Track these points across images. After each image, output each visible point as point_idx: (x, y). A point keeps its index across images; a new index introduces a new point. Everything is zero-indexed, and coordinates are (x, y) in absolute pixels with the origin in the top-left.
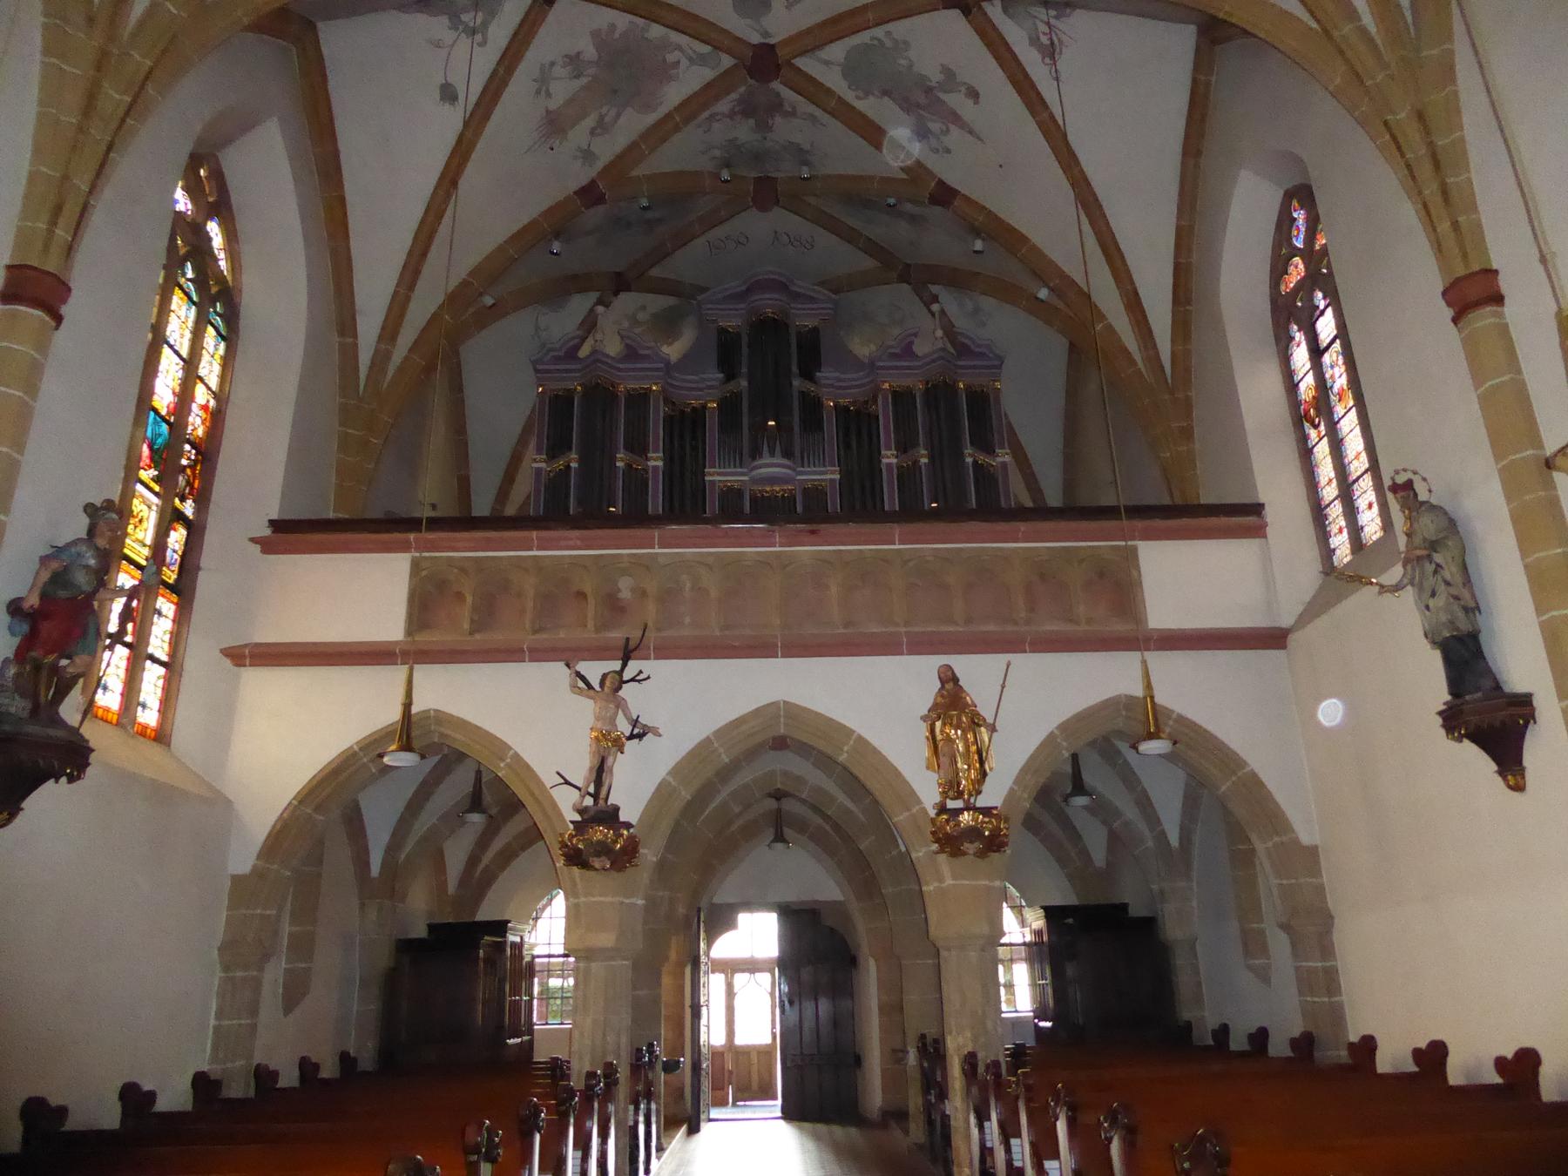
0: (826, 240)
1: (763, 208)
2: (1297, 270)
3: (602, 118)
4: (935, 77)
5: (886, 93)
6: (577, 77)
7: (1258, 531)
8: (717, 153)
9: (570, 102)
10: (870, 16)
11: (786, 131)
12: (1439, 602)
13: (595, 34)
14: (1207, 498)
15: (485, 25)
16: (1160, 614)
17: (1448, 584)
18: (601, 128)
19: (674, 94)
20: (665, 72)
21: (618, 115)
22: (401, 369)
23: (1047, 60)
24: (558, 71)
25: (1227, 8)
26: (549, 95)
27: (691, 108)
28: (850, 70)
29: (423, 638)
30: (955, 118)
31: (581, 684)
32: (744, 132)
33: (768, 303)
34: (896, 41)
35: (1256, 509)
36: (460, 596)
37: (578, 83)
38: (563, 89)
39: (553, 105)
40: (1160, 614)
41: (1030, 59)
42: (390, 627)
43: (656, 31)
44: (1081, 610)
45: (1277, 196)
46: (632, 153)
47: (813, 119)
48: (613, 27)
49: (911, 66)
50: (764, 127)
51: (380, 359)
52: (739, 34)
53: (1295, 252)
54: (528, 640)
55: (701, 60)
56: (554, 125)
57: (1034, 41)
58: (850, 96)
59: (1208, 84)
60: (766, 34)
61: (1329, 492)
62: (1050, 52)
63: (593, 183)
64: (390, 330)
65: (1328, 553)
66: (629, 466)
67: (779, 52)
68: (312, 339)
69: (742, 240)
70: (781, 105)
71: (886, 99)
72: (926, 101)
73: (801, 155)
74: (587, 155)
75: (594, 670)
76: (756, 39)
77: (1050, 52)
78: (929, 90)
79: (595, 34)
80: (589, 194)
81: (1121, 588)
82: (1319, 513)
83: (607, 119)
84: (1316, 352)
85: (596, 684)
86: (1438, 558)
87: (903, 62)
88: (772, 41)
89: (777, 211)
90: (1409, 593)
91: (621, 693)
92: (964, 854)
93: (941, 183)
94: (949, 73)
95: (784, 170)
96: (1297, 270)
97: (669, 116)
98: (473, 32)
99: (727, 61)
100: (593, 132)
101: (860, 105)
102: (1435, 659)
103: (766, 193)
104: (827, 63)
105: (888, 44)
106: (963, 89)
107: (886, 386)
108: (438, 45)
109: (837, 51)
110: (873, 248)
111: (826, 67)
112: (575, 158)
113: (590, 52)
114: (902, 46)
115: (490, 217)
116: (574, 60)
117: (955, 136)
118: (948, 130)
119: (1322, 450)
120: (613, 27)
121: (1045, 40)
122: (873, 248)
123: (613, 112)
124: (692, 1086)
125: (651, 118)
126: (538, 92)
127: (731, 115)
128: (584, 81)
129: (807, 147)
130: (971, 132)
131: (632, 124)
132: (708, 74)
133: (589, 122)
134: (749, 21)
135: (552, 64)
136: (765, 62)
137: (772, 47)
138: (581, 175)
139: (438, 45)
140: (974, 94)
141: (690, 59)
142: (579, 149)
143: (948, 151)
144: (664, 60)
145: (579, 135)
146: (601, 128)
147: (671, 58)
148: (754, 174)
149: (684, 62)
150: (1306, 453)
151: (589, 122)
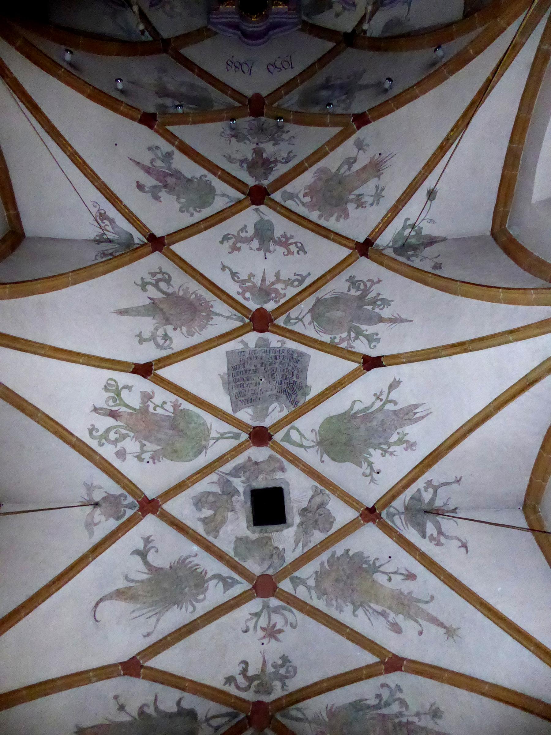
0: (216, 69)
1: (257, 96)
3: (349, 169)
4: (163, 194)
5: (190, 180)
6: (360, 195)
8: (285, 136)
9: (365, 182)
10: (202, 226)
11: (246, 150)
13: (347, 217)
15: (404, 228)
18: (350, 162)
19: (307, 178)
20: (311, 191)
21: (339, 169)
22: (516, 16)
23: (103, 212)
24: (370, 200)
25: (7, 290)
26: (377, 187)
28: (212, 191)
30: (148, 171)
32: (269, 149)
33: (254, 25)
34: (188, 211)
38: (368, 189)
41: (112, 212)
47: (230, 159)
48: (338, 220)
49: (178, 199)
50: (258, 152)
51: (525, 32)
52: (271, 211)
55: (292, 196)
56: (376, 167)
57: (112, 221)
58: (210, 176)
59: (7, 210)
60: (256, 210)
62: (103, 216)
63: (359, 128)
64: (514, 49)
67: (250, 202)
69: (271, 68)
70: (248, 168)
71: (189, 176)
72: (166, 181)
73: (236, 134)
74: (360, 146)
76: (262, 208)
79: (347, 217)
80: (362, 120)
83: (346, 167)
87: (183, 200)
88: (254, 207)
89: (249, 92)
92: (305, 195)
93: (151, 127)
94: (157, 198)
95: (245, 122)
97: (311, 166)
98: (413, 226)
100: (355, 160)
101: (204, 172)
103: (256, 106)
104: (224, 195)
105: (191, 209)
106: (147, 189)
109: (219, 204)
110: (189, 65)
111: (224, 195)
112: (368, 145)
113: (351, 207)
115: (424, 118)
116: (360, 204)
118: (151, 163)
120: (338, 220)
122: (189, 65)
123: (342, 171)
124: (233, 457)
125: (321, 164)
126: (383, 189)
127: (276, 162)
128: (357, 192)
129: (233, 140)
130: (138, 163)
131: (332, 162)
132: (288, 188)
133: (356, 167)
134: (266, 218)
135: (372, 205)
136: (258, 196)
137: (253, 203)
138: (366, 132)
140: (140, 187)
141: (297, 197)
142: (364, 150)
143: (150, 149)
144: (312, 198)
145: (363, 160)
146: (350, 162)
147: (308, 199)
148: (263, 119)
149: (301, 195)
151: (356, 167)
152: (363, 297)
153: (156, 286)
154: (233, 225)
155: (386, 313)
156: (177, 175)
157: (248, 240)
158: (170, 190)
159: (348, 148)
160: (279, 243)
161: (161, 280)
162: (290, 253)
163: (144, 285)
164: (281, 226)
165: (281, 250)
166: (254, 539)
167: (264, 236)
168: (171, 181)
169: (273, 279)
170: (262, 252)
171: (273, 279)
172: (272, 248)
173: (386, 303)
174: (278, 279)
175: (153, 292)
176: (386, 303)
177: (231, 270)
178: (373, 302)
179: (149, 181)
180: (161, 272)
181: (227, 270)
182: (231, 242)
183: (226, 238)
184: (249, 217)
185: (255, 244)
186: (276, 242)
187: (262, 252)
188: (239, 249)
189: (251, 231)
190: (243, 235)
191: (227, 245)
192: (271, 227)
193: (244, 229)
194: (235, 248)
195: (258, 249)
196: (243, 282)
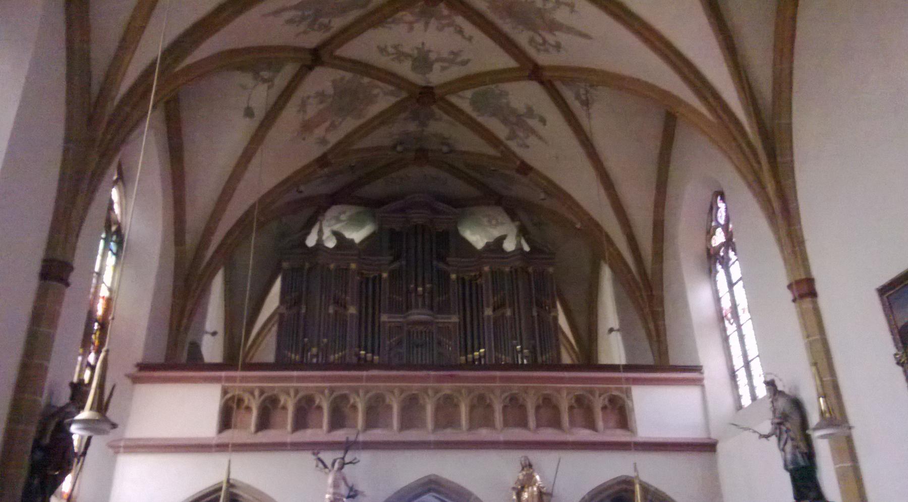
2: (719, 238)
6: (321, 102)
7: (698, 382)
12: (789, 447)
14: (672, 362)
16: (645, 431)
17: (792, 439)
27: (384, 118)
28: (473, 103)
29: (229, 436)
30: (533, 131)
31: (321, 465)
32: (412, 127)
35: (697, 369)
36: (248, 409)
37: (321, 107)
38: (312, 110)
39: (307, 117)
40: (647, 426)
41: (575, 106)
42: (206, 426)
43: (366, 80)
44: (600, 424)
45: (709, 194)
46: (349, 138)
48: (342, 79)
53: (718, 225)
54: (290, 438)
55: (392, 93)
56: (307, 127)
57: (578, 97)
58: (474, 115)
61: (738, 362)
62: (586, 104)
65: (738, 398)
66: (336, 312)
68: (164, 249)
72: (518, 121)
73: (444, 141)
75: (328, 457)
76: (423, 84)
77: (586, 104)
78: (519, 116)
80: (322, 161)
81: (621, 414)
82: (733, 375)
84: (731, 285)
85: (329, 463)
86: (788, 425)
90: (774, 439)
91: (343, 470)
92: (376, 96)
96: (719, 238)
99: (404, 95)
100: (327, 130)
101: (480, 119)
102: (786, 478)
107: (486, 269)
108: (244, 87)
109: (468, 94)
113: (331, 91)
114: (504, 94)
117: (532, 140)
119: (734, 341)
121: (583, 97)
131: (349, 124)
132: (393, 100)
133: (327, 124)
135: (309, 97)
137: (432, 88)
138: (317, 152)
139: (244, 87)
140: (543, 121)
143: (528, 147)
145: (319, 132)
146: (333, 126)
147: (376, 91)
150: (726, 339)
152: (315, 20)
153: (545, 42)
154: (455, 72)
155: (287, 15)
156: (505, 121)
157: (438, 60)
158: (514, 111)
159: (334, 138)
160: (407, 56)
161: (540, 45)
162: (395, 47)
163: (558, 46)
164: (405, 69)
165: (407, 49)
166: (508, 20)
167: (423, 61)
168: (513, 119)
169: (416, 26)
170: (426, 49)
171: (416, 26)
172: (416, 52)
173: (290, 21)
174: (411, 24)
175: (551, 39)
176: (290, 21)
177: (463, 36)
178: (303, 18)
179: (533, 123)
180: (538, 50)
181: (467, 36)
182: (459, 59)
183: (465, 63)
184: (436, 77)
185: (433, 56)
186: (410, 56)
187: (426, 49)
188: (452, 53)
189: (437, 66)
190: (446, 64)
191: (464, 57)
192: (414, 68)
193: (443, 69)
194: (455, 54)
195: (430, 51)
196: (449, 25)
